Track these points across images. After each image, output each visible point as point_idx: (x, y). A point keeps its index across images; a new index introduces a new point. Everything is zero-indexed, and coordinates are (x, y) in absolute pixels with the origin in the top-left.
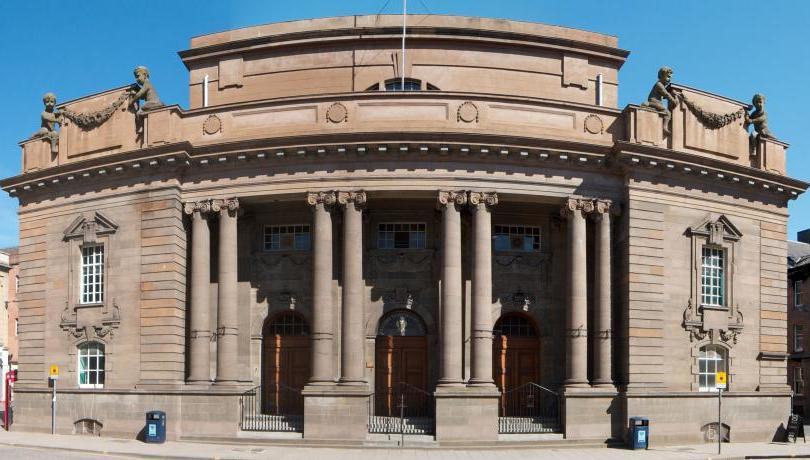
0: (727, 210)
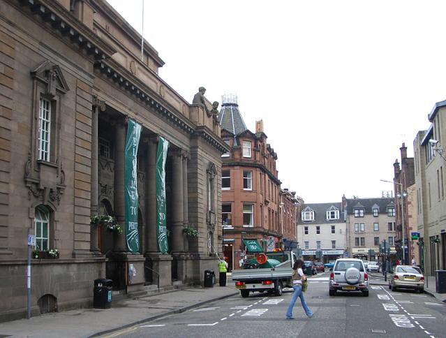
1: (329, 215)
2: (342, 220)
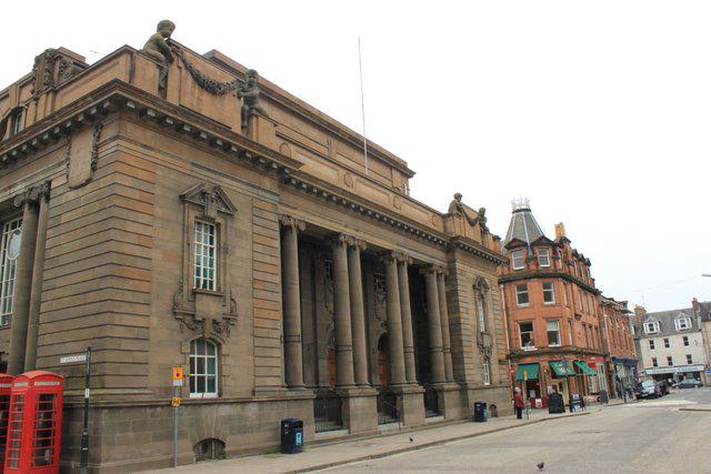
0: (226, 183)
1: (678, 324)
2: (695, 329)
